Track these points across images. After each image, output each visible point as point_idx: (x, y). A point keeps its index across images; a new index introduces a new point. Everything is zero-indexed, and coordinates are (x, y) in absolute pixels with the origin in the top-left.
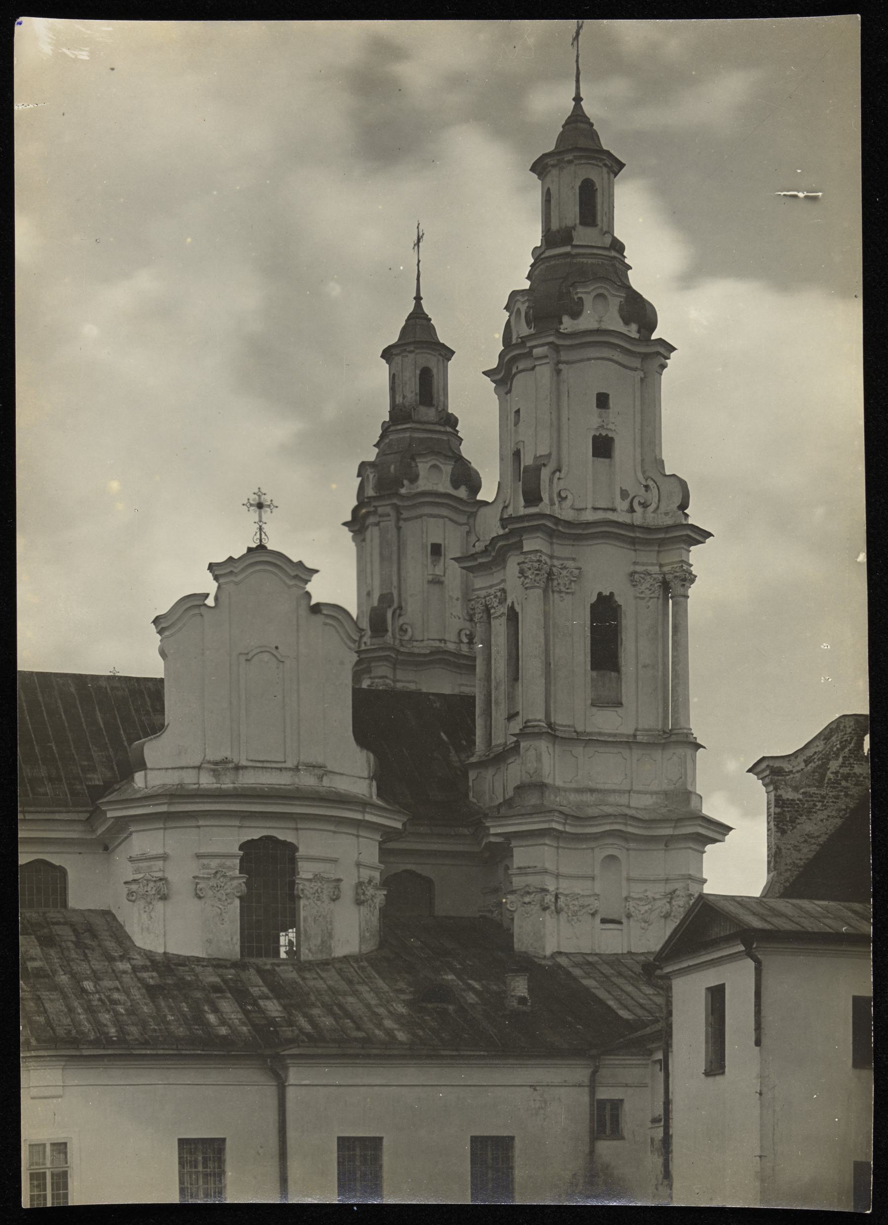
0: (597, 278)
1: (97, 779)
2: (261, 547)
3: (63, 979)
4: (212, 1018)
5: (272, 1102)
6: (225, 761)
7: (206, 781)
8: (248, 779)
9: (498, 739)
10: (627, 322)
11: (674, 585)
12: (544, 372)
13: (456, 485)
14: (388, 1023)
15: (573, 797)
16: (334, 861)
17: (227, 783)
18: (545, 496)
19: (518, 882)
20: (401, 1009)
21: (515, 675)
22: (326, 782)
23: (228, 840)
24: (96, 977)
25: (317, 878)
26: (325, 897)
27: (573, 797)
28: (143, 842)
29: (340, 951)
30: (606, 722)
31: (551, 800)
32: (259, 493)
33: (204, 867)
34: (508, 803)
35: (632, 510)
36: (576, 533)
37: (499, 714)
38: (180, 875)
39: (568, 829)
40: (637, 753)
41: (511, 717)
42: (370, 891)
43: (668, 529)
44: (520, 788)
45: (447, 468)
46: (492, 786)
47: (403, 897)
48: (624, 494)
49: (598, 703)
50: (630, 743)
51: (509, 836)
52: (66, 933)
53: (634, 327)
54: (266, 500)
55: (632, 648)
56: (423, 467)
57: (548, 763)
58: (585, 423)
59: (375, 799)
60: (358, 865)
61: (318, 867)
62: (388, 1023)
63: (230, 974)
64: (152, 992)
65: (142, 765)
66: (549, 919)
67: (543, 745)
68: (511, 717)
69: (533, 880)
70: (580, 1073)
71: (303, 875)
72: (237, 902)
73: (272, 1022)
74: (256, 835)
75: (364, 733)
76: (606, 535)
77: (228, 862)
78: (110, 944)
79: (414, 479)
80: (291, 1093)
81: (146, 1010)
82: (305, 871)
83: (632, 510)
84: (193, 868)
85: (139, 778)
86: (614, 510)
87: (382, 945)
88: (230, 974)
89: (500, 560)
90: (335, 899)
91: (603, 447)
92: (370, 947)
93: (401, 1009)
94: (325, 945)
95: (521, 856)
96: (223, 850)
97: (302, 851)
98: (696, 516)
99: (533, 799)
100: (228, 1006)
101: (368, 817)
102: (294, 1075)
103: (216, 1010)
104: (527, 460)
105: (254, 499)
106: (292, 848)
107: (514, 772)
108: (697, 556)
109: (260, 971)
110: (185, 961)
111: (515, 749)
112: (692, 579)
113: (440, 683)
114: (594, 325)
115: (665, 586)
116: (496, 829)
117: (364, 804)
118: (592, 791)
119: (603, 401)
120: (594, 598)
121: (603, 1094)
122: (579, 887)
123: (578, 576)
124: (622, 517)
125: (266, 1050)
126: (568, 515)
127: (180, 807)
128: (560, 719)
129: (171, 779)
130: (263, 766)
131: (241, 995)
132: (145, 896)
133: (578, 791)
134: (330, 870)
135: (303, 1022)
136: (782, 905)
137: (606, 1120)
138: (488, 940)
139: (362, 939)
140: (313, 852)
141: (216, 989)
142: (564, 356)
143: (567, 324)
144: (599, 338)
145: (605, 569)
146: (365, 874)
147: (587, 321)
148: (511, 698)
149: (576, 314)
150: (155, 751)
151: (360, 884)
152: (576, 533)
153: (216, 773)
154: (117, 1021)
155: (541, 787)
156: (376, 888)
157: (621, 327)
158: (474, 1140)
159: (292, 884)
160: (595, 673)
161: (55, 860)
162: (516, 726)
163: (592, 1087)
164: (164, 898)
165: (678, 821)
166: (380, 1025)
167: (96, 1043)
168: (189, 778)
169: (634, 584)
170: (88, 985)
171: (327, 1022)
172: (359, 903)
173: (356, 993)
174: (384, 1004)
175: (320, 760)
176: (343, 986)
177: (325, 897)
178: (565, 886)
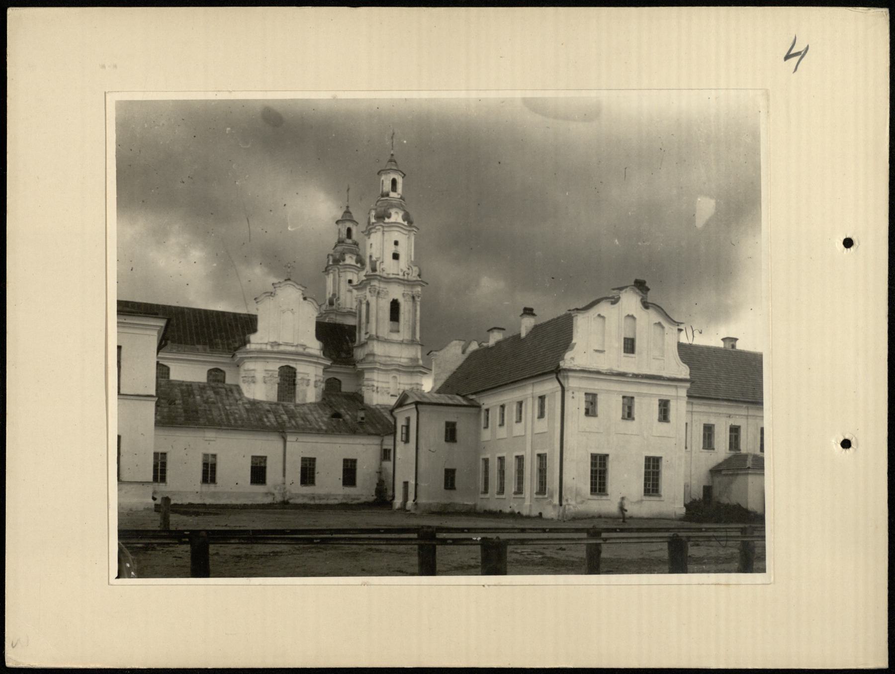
1: (237, 345)
3: (220, 405)
4: (265, 420)
6: (275, 342)
7: (269, 348)
8: (282, 348)
9: (363, 340)
12: (379, 234)
13: (357, 262)
14: (321, 424)
15: (384, 359)
17: (275, 349)
18: (378, 269)
19: (366, 383)
20: (325, 419)
21: (368, 322)
23: (275, 366)
24: (230, 405)
25: (302, 379)
27: (384, 359)
28: (249, 365)
30: (395, 337)
31: (377, 359)
34: (364, 359)
36: (387, 280)
37: (363, 332)
38: (259, 375)
40: (404, 346)
41: (366, 333)
42: (319, 384)
44: (368, 355)
45: (354, 257)
46: (359, 354)
47: (331, 386)
49: (392, 331)
50: (401, 343)
51: (363, 369)
52: (223, 390)
56: (347, 257)
57: (378, 349)
62: (321, 424)
63: (274, 406)
64: (247, 410)
65: (249, 342)
66: (375, 394)
67: (375, 343)
68: (366, 333)
69: (370, 383)
70: (376, 441)
73: (284, 422)
75: (319, 336)
76: (395, 282)
78: (237, 396)
79: (344, 260)
80: (288, 443)
81: (245, 416)
82: (299, 377)
85: (248, 346)
87: (324, 399)
88: (274, 406)
89: (364, 287)
91: (396, 256)
92: (319, 400)
93: (325, 419)
94: (304, 399)
95: (367, 376)
99: (371, 358)
100: (271, 416)
103: (267, 417)
104: (374, 259)
107: (366, 350)
109: (283, 406)
110: (260, 402)
111: (366, 343)
113: (350, 321)
116: (359, 366)
117: (318, 357)
119: (396, 243)
121: (385, 447)
122: (384, 385)
123: (387, 293)
124: (401, 277)
125: (281, 430)
126: (385, 275)
127: (262, 355)
128: (380, 335)
129: (258, 347)
130: (286, 344)
131: (275, 413)
134: (306, 377)
135: (293, 422)
136: (436, 395)
137: (386, 455)
138: (356, 399)
141: (268, 411)
142: (386, 229)
143: (387, 220)
144: (396, 224)
146: (318, 378)
147: (392, 220)
148: (366, 328)
149: (389, 217)
150: (253, 338)
152: (387, 280)
153: (272, 346)
154: (235, 419)
155: (373, 355)
158: (739, 427)
159: (294, 380)
161: (222, 368)
162: (367, 336)
163: (381, 445)
164: (254, 382)
165: (414, 367)
166: (317, 424)
167: (228, 426)
168: (264, 347)
170: (228, 407)
171: (301, 422)
172: (315, 387)
173: (312, 414)
174: (322, 418)
176: (308, 411)
178: (380, 385)
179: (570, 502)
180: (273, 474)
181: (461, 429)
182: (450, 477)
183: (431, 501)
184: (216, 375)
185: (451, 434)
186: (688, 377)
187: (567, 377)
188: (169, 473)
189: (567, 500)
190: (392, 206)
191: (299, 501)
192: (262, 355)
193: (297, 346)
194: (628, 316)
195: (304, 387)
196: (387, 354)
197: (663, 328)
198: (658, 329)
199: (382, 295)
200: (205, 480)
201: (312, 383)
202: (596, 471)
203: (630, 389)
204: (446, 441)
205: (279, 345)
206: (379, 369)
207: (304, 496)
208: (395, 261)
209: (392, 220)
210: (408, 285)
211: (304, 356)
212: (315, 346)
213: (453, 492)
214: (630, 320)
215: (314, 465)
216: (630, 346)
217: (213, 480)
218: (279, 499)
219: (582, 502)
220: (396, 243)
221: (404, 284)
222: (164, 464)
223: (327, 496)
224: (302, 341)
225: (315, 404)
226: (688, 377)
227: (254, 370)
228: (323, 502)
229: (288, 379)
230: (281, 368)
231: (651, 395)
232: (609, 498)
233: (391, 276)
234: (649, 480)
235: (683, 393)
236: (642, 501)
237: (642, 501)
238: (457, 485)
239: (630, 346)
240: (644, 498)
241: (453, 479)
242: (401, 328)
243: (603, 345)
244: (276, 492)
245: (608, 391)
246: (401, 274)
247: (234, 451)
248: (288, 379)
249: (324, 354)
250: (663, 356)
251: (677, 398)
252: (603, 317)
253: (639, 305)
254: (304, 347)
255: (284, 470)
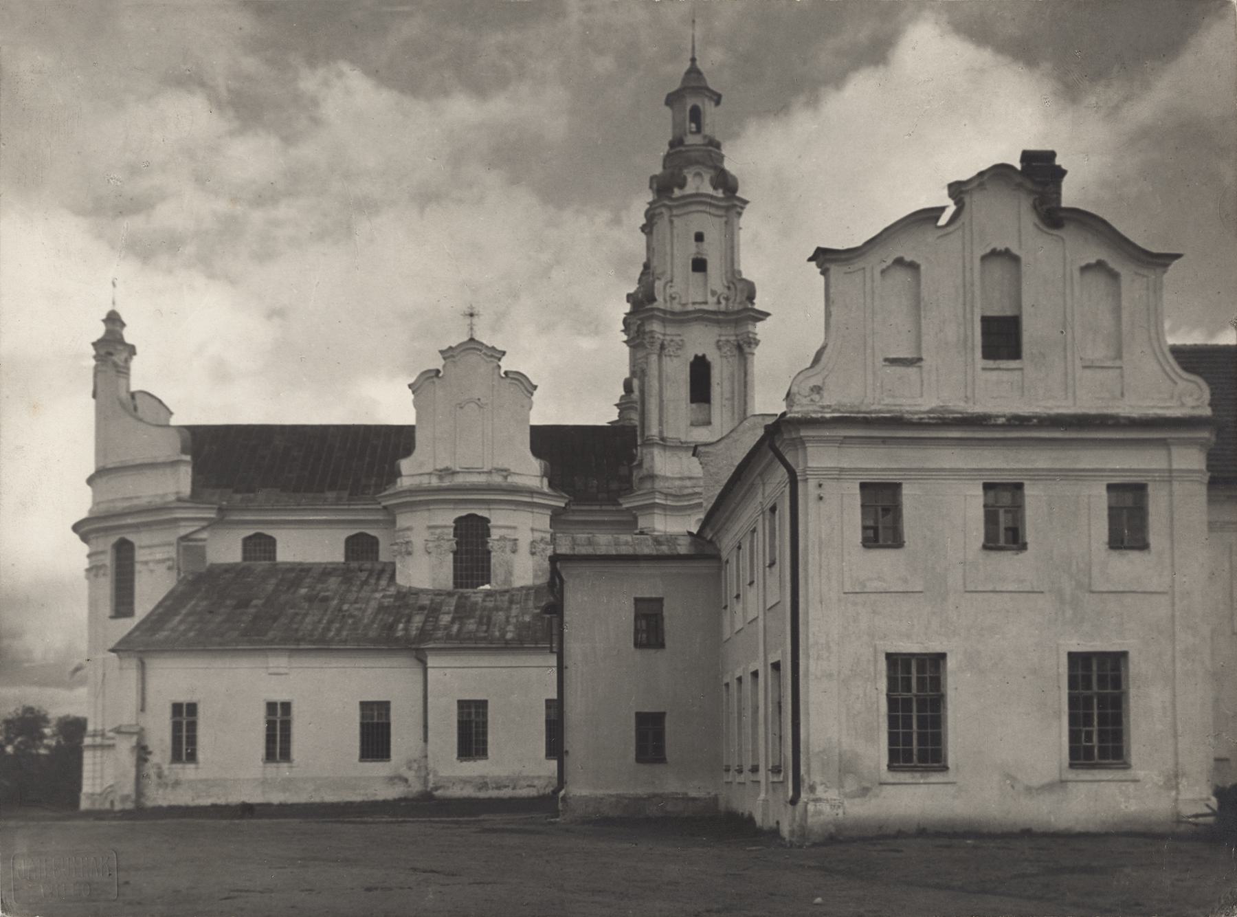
0: (697, 162)
2: (472, 340)
5: (420, 678)
6: (447, 469)
7: (435, 482)
8: (459, 480)
10: (715, 188)
11: (743, 348)
15: (677, 483)
16: (515, 528)
17: (447, 483)
22: (510, 479)
23: (447, 518)
25: (503, 538)
26: (508, 549)
27: (677, 483)
29: (518, 583)
32: (472, 308)
33: (432, 534)
35: (719, 302)
36: (682, 318)
39: (669, 503)
42: (542, 546)
43: (738, 312)
48: (714, 293)
53: (720, 191)
54: (475, 311)
55: (719, 389)
58: (685, 251)
59: (546, 489)
60: (532, 530)
61: (503, 532)
67: (656, 451)
71: (493, 537)
72: (451, 555)
74: (464, 513)
75: (536, 450)
76: (696, 319)
77: (446, 531)
80: (430, 671)
82: (495, 534)
83: (719, 302)
84: (426, 535)
86: (706, 303)
90: (514, 552)
91: (699, 265)
94: (507, 580)
96: (443, 523)
97: (493, 523)
98: (759, 304)
99: (648, 485)
101: (536, 500)
102: (431, 661)
105: (468, 311)
106: (487, 521)
108: (760, 328)
112: (757, 343)
114: (694, 192)
115: (740, 348)
117: (532, 492)
118: (690, 478)
119: (699, 237)
120: (692, 359)
124: (711, 307)
126: (677, 308)
127: (423, 498)
128: (670, 434)
130: (469, 471)
132: (400, 553)
133: (681, 479)
139: (536, 576)
140: (501, 523)
142: (675, 212)
143: (677, 192)
145: (702, 341)
146: (538, 535)
147: (690, 189)
149: (682, 186)
150: (405, 465)
151: (533, 542)
152: (682, 318)
153: (441, 478)
156: (547, 543)
157: (710, 191)
160: (694, 405)
168: (425, 481)
169: (719, 348)
172: (533, 554)
175: (506, 466)
177: (508, 549)
179: (820, 791)
180: (403, 739)
181: (674, 617)
182: (650, 735)
183: (600, 792)
184: (361, 547)
185: (649, 627)
186: (1207, 412)
187: (801, 443)
188: (495, 737)
189: (812, 789)
190: (691, 163)
191: (456, 792)
192: (423, 498)
193: (490, 473)
194: (994, 253)
195: (508, 555)
196: (686, 474)
197: (1114, 276)
198: (1098, 282)
199: (670, 350)
200: (270, 756)
201: (524, 547)
202: (907, 702)
203: (1000, 462)
204: (638, 645)
205: (454, 473)
206: (664, 508)
207: (465, 781)
208: (698, 275)
209: (690, 189)
210: (728, 322)
211: (514, 496)
212: (530, 471)
213: (658, 768)
214: (998, 270)
215: (485, 715)
216: (1002, 339)
217: (286, 756)
218: (416, 787)
219: (864, 792)
220: (699, 237)
221: (718, 322)
222: (286, 726)
223: (514, 782)
224: (501, 463)
225: (528, 588)
226: (1207, 412)
227: (409, 529)
228: (506, 793)
229: (472, 547)
230: (458, 521)
231: (1095, 473)
232: (950, 776)
233: (690, 308)
234: (1088, 720)
235: (1191, 459)
236: (1063, 782)
237: (1063, 782)
238: (669, 751)
239: (1002, 339)
240: (1071, 775)
241: (659, 736)
242: (716, 418)
243: (919, 347)
244: (410, 775)
245: (925, 474)
246: (712, 300)
247: (328, 691)
248: (472, 547)
249: (551, 485)
250: (1119, 356)
251: (1169, 476)
252: (914, 267)
253: (1029, 220)
254: (506, 472)
255: (426, 727)
